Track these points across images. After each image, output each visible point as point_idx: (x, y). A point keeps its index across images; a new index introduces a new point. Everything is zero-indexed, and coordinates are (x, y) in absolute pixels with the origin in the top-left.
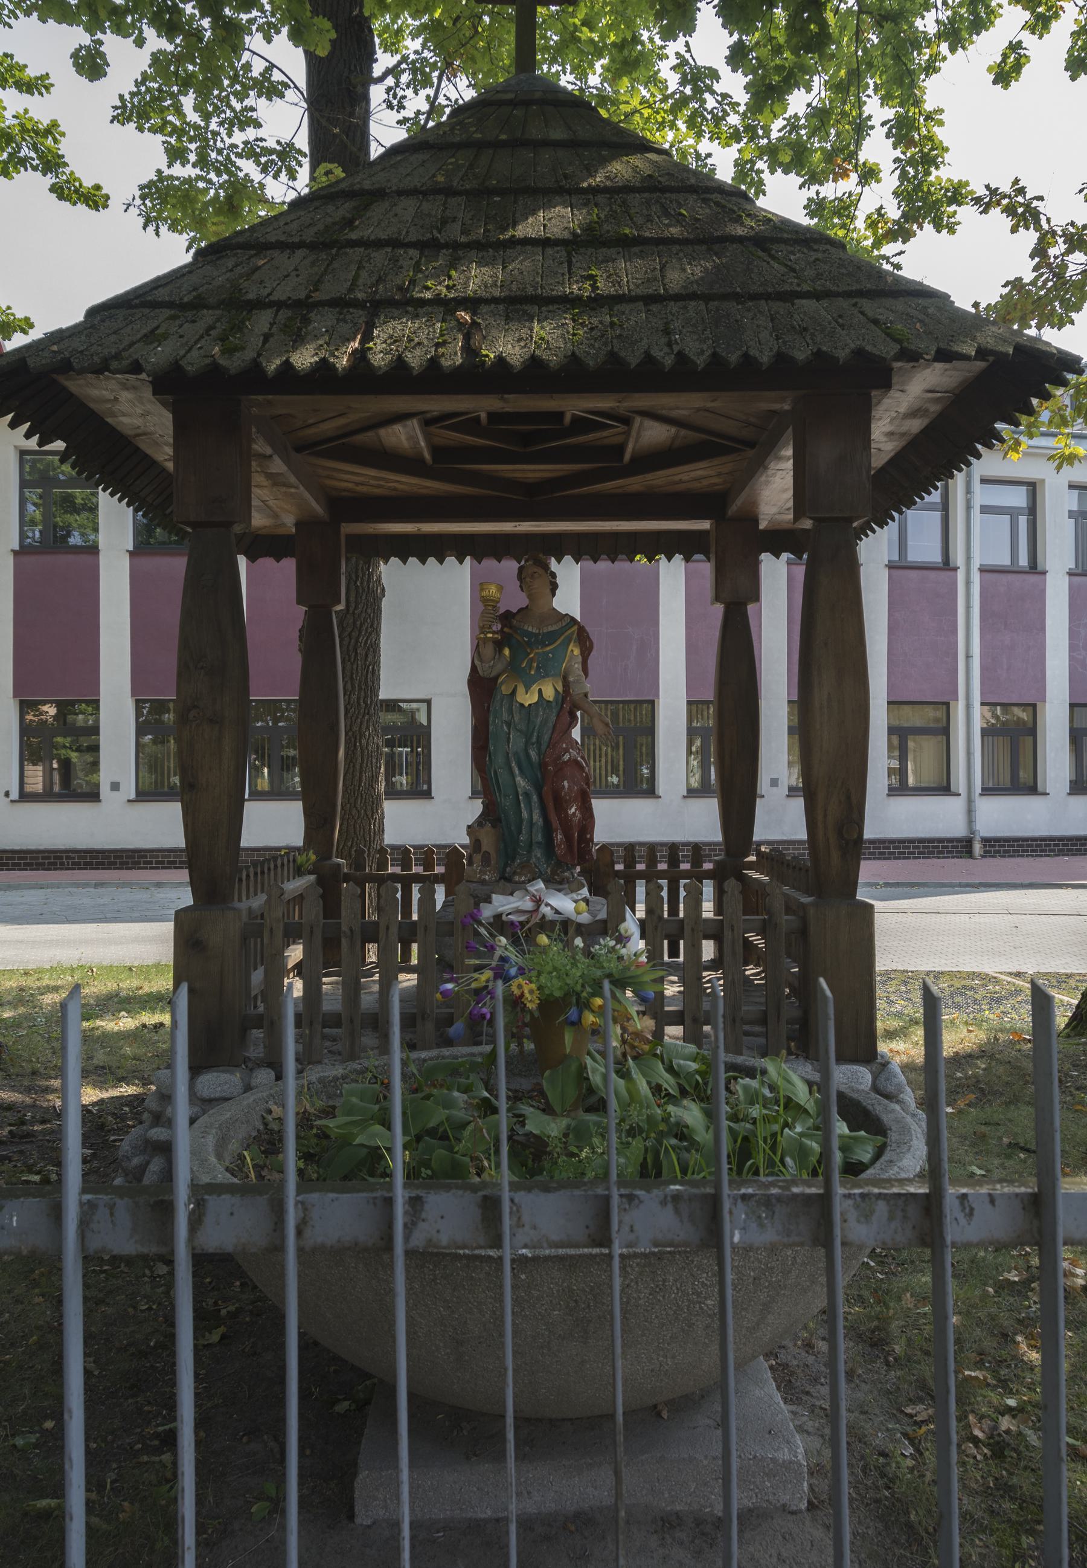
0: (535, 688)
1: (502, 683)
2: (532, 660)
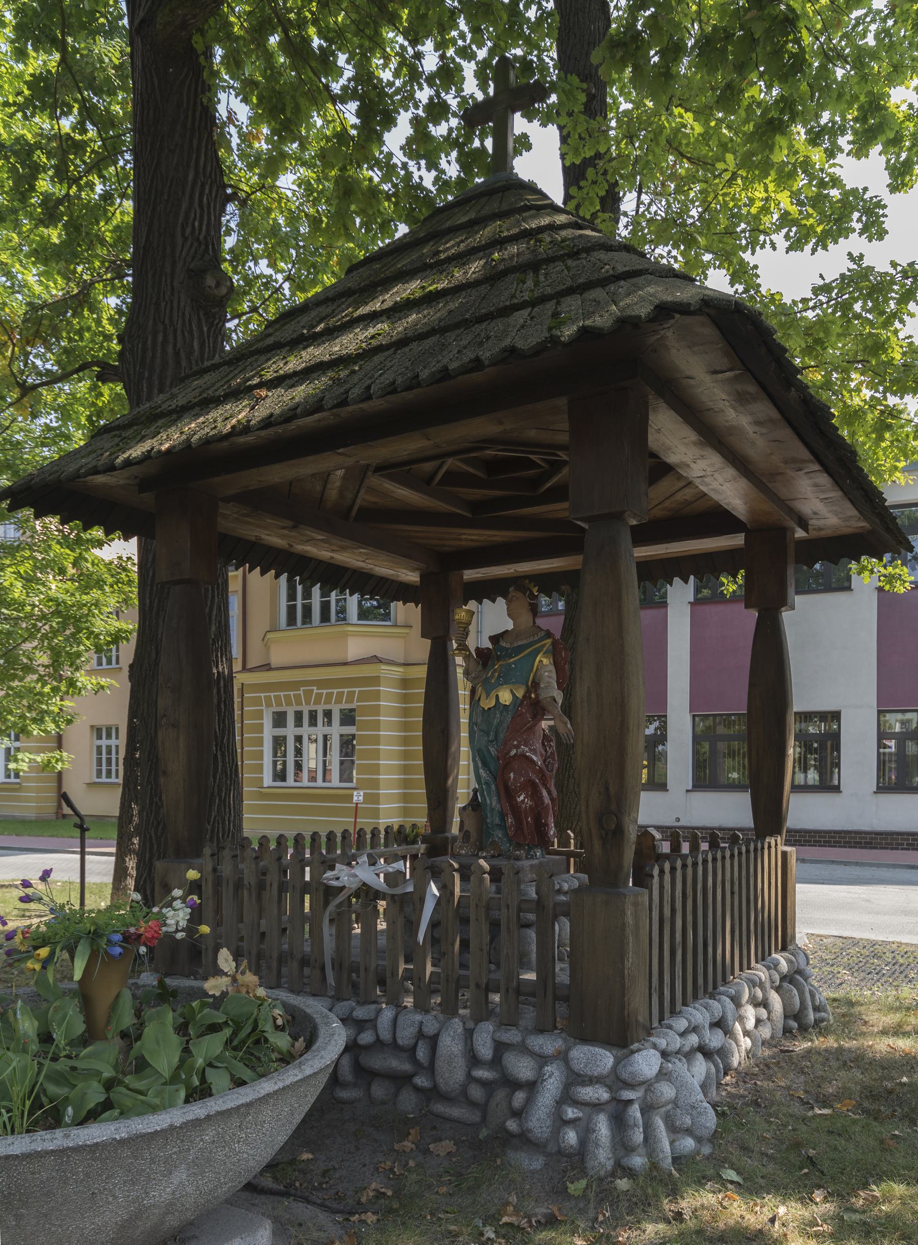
0: (493, 694)
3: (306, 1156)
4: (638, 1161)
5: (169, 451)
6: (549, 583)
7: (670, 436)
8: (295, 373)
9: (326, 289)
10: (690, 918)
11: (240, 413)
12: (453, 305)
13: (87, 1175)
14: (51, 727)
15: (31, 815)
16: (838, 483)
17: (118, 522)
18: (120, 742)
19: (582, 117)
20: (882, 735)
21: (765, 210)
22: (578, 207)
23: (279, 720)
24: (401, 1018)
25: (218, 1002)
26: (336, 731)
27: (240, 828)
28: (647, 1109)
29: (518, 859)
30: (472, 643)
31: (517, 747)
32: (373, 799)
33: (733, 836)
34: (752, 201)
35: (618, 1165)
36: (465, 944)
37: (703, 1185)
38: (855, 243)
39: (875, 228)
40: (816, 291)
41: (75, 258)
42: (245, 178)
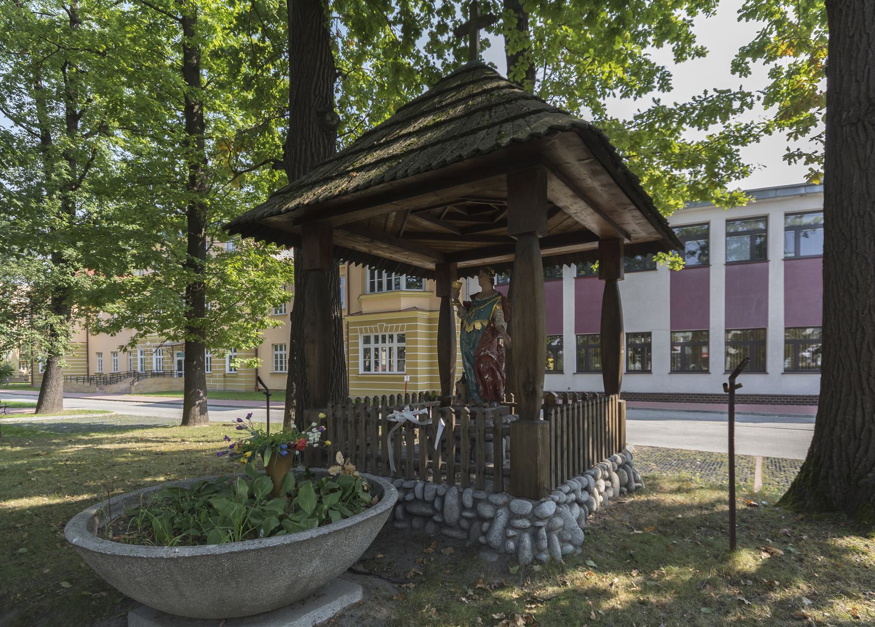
0: (472, 324)
3: (380, 556)
4: (545, 557)
5: (308, 204)
6: (500, 268)
7: (558, 193)
8: (370, 164)
9: (386, 121)
10: (571, 436)
11: (343, 184)
12: (448, 129)
13: (271, 562)
14: (252, 345)
15: (243, 389)
16: (645, 215)
17: (284, 241)
18: (287, 352)
19: (516, 31)
20: (673, 344)
21: (610, 77)
22: (514, 76)
23: (367, 340)
24: (426, 487)
25: (335, 478)
26: (395, 345)
27: (347, 393)
28: (549, 531)
29: (485, 407)
30: (461, 299)
31: (484, 351)
32: (415, 379)
33: (594, 395)
34: (603, 73)
35: (535, 558)
36: (458, 450)
37: (577, 568)
38: (656, 93)
39: (666, 86)
40: (636, 118)
41: (260, 106)
42: (345, 65)
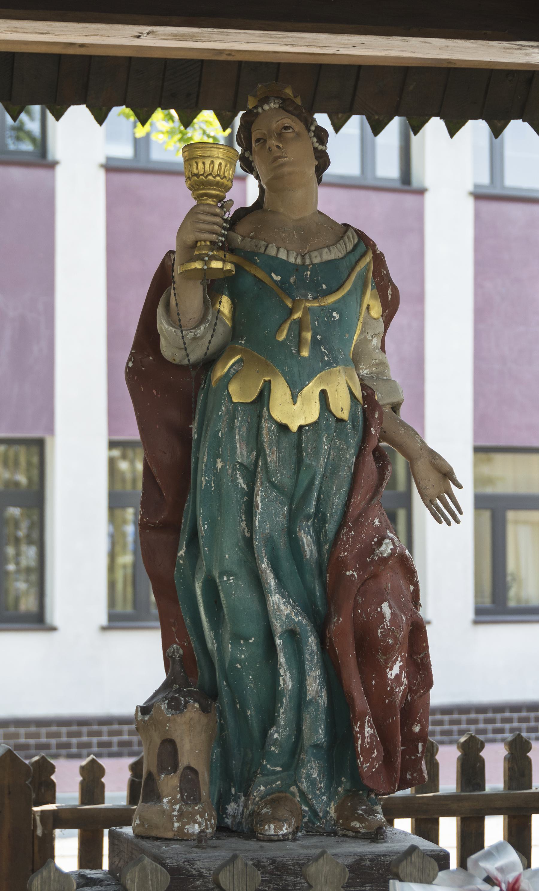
0: (312, 390)
1: (227, 379)
2: (300, 325)
